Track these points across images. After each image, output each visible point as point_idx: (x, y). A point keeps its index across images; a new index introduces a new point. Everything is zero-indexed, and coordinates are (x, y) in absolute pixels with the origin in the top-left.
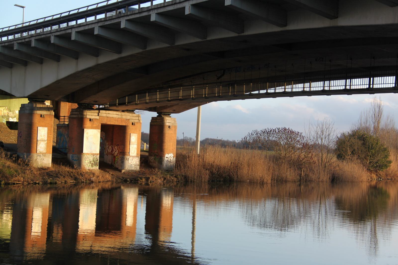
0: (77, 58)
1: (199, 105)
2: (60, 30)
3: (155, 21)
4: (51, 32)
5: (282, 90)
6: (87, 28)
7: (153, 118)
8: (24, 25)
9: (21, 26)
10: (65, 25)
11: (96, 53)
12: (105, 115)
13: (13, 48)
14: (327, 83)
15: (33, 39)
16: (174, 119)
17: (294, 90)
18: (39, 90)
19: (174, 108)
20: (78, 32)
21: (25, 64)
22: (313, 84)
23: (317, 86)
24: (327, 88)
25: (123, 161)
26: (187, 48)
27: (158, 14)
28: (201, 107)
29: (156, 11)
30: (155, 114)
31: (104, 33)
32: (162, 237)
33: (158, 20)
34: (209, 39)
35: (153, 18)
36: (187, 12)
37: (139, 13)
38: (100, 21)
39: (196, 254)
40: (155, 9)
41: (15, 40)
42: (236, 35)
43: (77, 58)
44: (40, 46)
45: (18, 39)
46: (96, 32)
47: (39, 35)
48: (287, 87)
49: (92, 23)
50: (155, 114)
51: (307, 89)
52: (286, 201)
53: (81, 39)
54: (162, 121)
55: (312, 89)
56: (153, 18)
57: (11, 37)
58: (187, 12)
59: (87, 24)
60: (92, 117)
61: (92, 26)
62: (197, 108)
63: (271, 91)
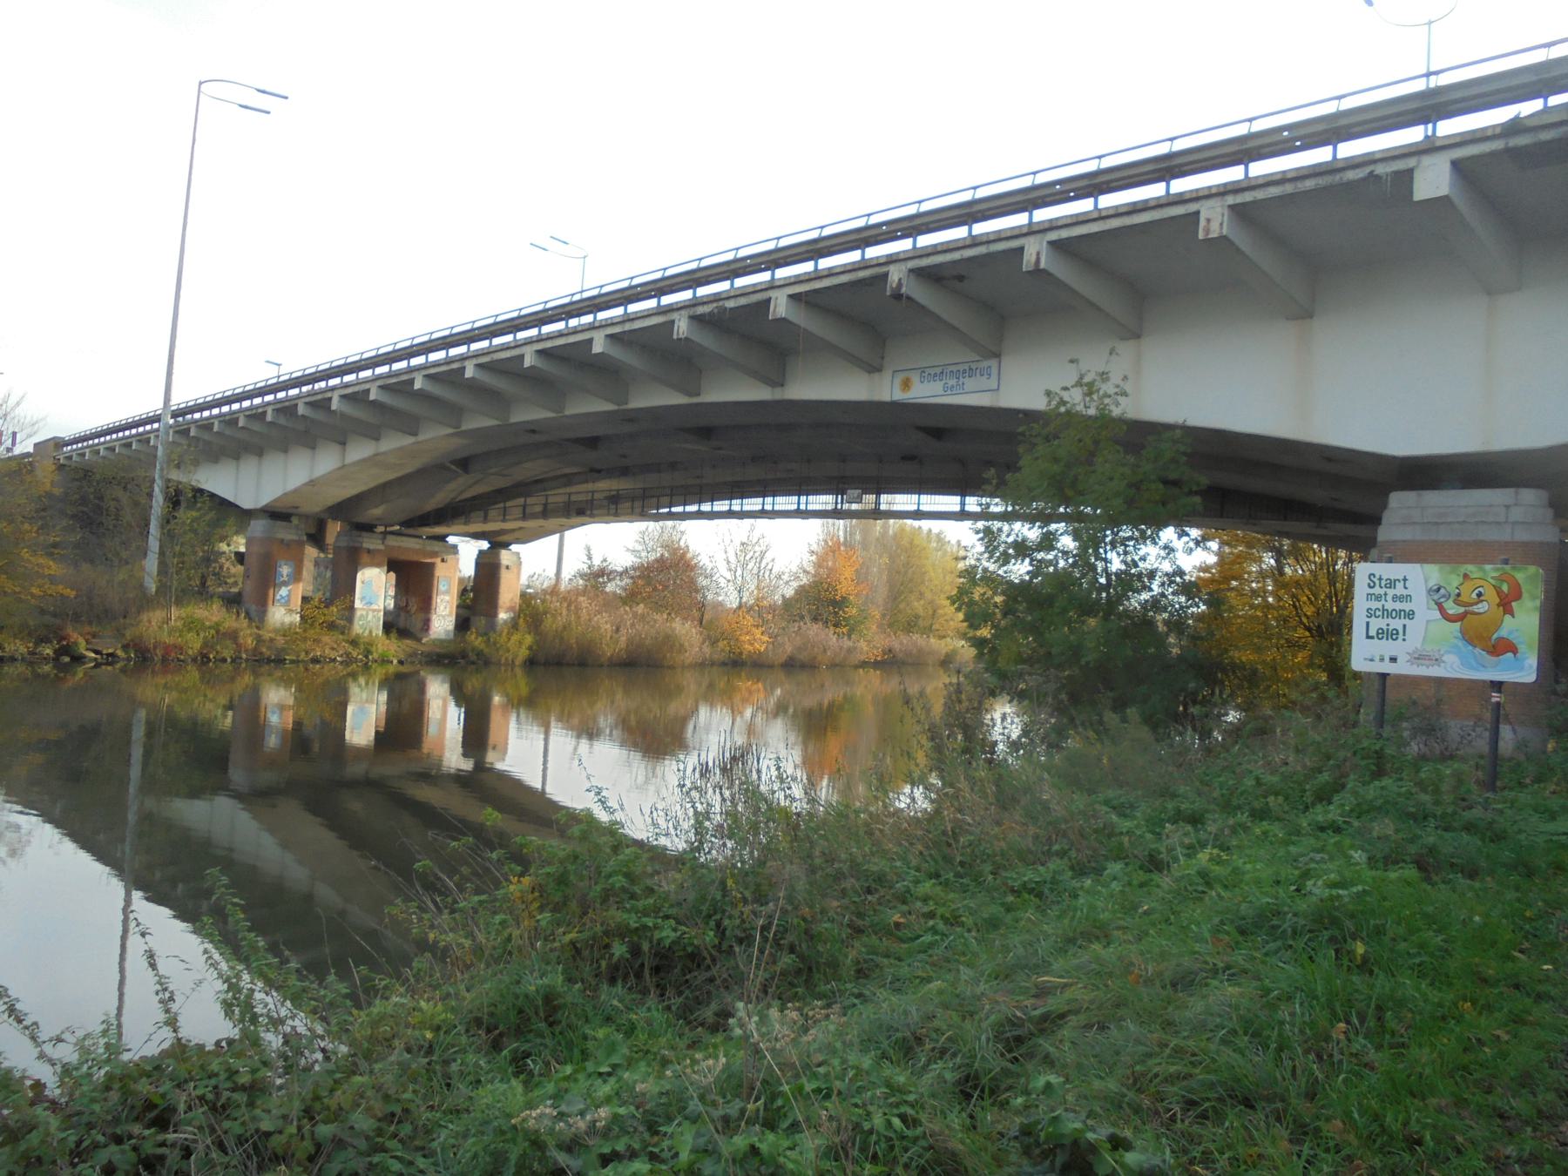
0: (313, 448)
1: (561, 530)
2: (202, 419)
3: (602, 353)
4: (298, 397)
5: (726, 508)
6: (356, 389)
7: (481, 552)
8: (282, 379)
9: (275, 381)
10: (323, 384)
11: (374, 434)
12: (395, 544)
13: (237, 423)
14: (803, 499)
15: (269, 410)
16: (518, 554)
17: (746, 508)
18: (279, 498)
19: (516, 535)
20: (343, 397)
21: (259, 452)
22: (779, 499)
23: (753, 504)
24: (803, 507)
25: (427, 623)
26: (532, 429)
27: (478, 366)
28: (568, 534)
29: (475, 361)
30: (485, 545)
31: (385, 398)
32: (491, 757)
33: (477, 376)
34: (568, 412)
35: (598, 347)
36: (527, 362)
37: (623, 322)
38: (380, 377)
39: (548, 789)
40: (601, 327)
41: (241, 410)
42: (616, 408)
43: (313, 448)
44: (282, 421)
45: (247, 409)
46: (372, 397)
47: (281, 401)
48: (734, 502)
49: (366, 381)
50: (485, 545)
51: (768, 507)
52: (522, 711)
53: (348, 409)
54: (497, 556)
55: (777, 508)
56: (598, 347)
57: (206, 414)
58: (527, 362)
59: (358, 383)
60: (372, 547)
61: (366, 386)
62: (557, 536)
63: (706, 507)
